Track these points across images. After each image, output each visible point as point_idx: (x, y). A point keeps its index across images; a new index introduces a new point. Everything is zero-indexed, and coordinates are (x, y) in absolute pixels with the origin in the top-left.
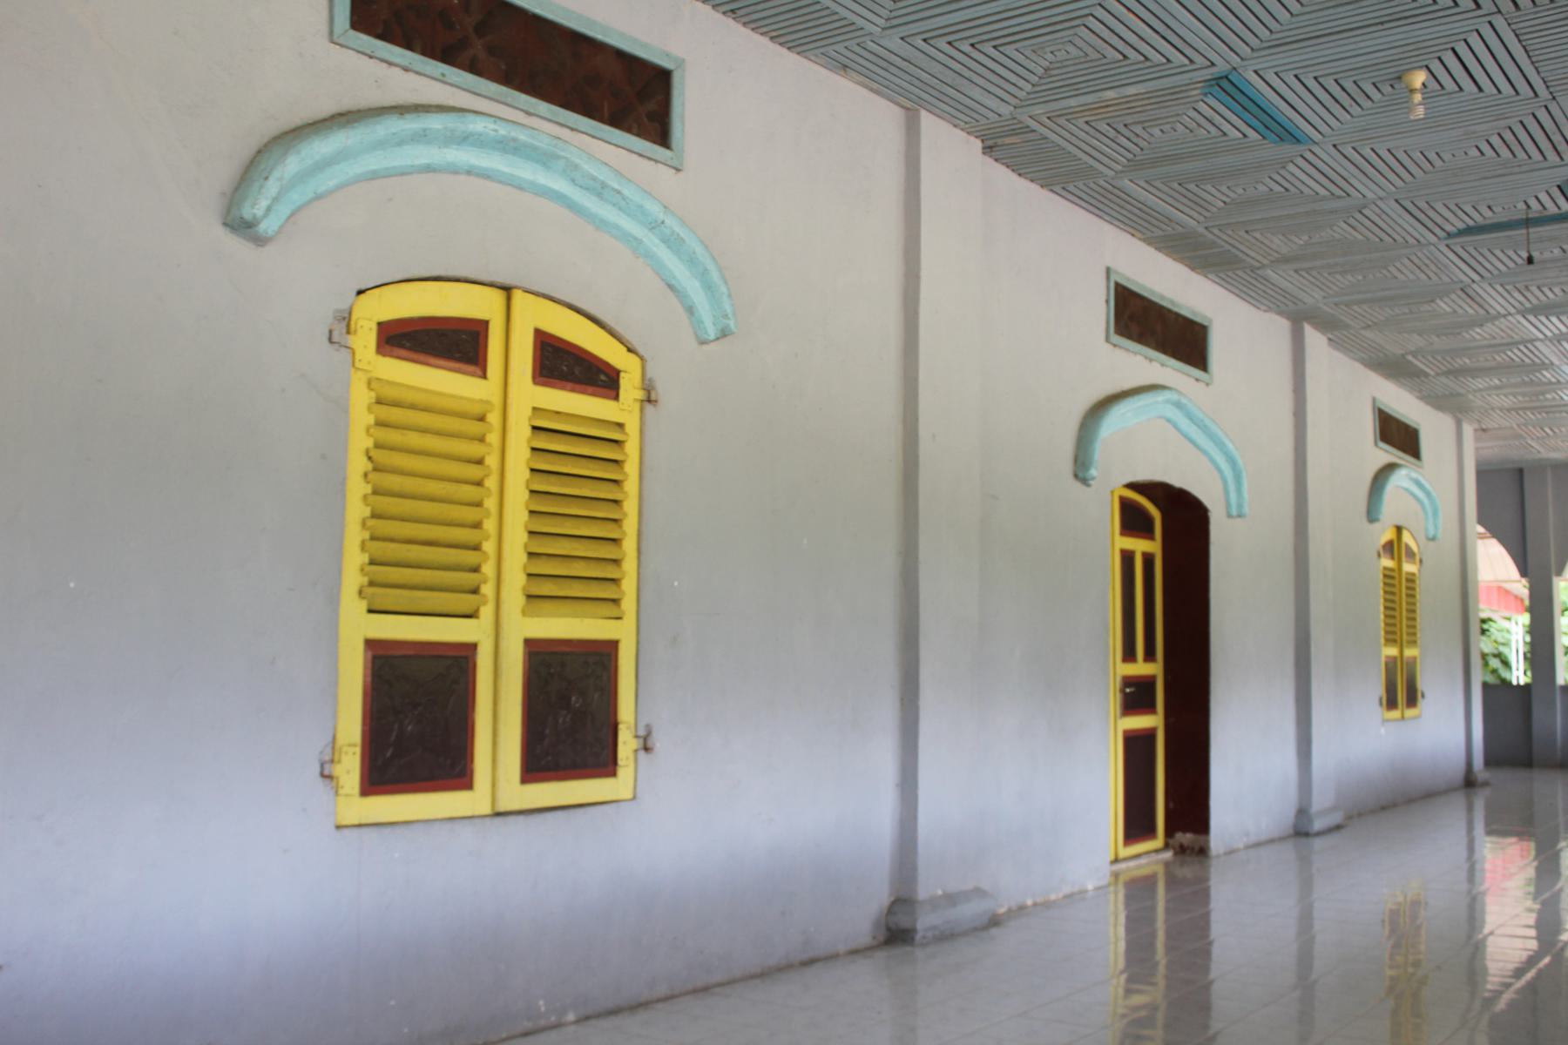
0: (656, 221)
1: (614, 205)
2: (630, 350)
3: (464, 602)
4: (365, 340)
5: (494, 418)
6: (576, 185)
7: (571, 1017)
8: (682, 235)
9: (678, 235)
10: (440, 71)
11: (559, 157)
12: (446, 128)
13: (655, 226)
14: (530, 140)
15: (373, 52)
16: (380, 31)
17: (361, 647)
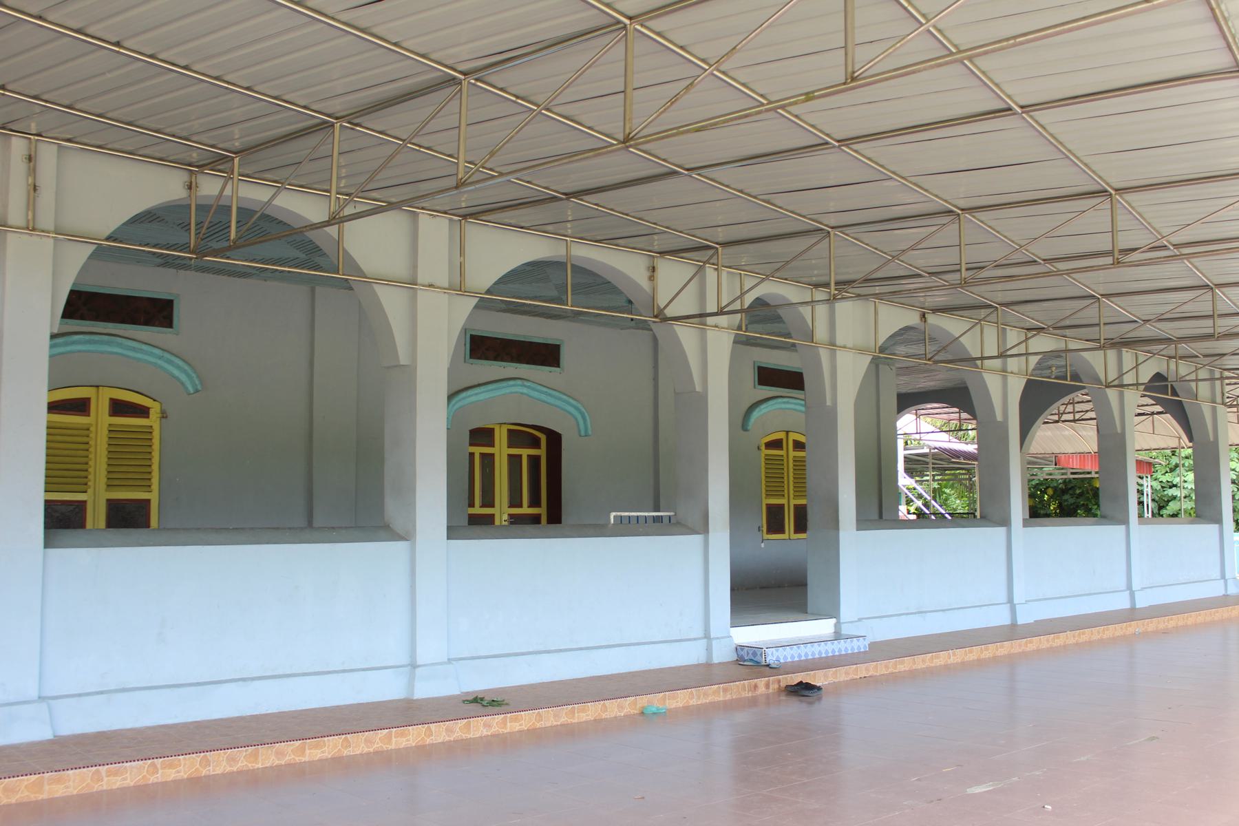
2: (155, 400)
3: (82, 488)
4: (763, 447)
5: (92, 429)
7: (786, 585)
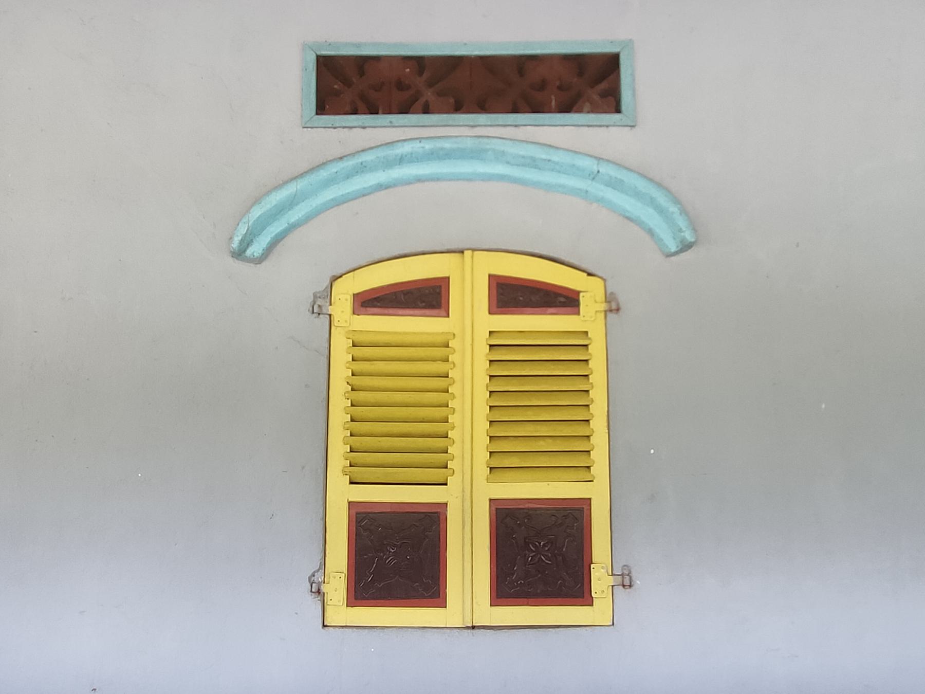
0: (593, 172)
1: (553, 170)
2: (589, 274)
6: (512, 165)
8: (619, 177)
9: (616, 178)
10: (388, 120)
11: (486, 151)
12: (378, 157)
13: (594, 176)
14: (455, 146)
15: (333, 125)
16: (348, 108)
17: (346, 505)
